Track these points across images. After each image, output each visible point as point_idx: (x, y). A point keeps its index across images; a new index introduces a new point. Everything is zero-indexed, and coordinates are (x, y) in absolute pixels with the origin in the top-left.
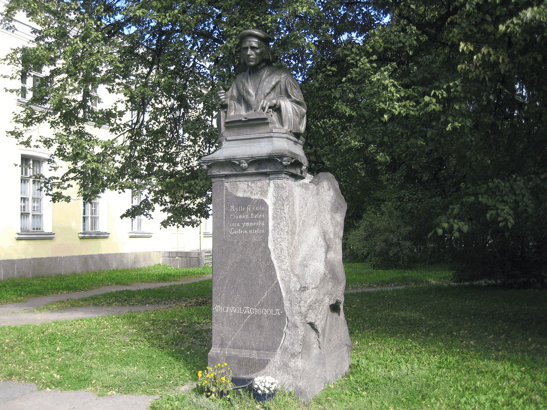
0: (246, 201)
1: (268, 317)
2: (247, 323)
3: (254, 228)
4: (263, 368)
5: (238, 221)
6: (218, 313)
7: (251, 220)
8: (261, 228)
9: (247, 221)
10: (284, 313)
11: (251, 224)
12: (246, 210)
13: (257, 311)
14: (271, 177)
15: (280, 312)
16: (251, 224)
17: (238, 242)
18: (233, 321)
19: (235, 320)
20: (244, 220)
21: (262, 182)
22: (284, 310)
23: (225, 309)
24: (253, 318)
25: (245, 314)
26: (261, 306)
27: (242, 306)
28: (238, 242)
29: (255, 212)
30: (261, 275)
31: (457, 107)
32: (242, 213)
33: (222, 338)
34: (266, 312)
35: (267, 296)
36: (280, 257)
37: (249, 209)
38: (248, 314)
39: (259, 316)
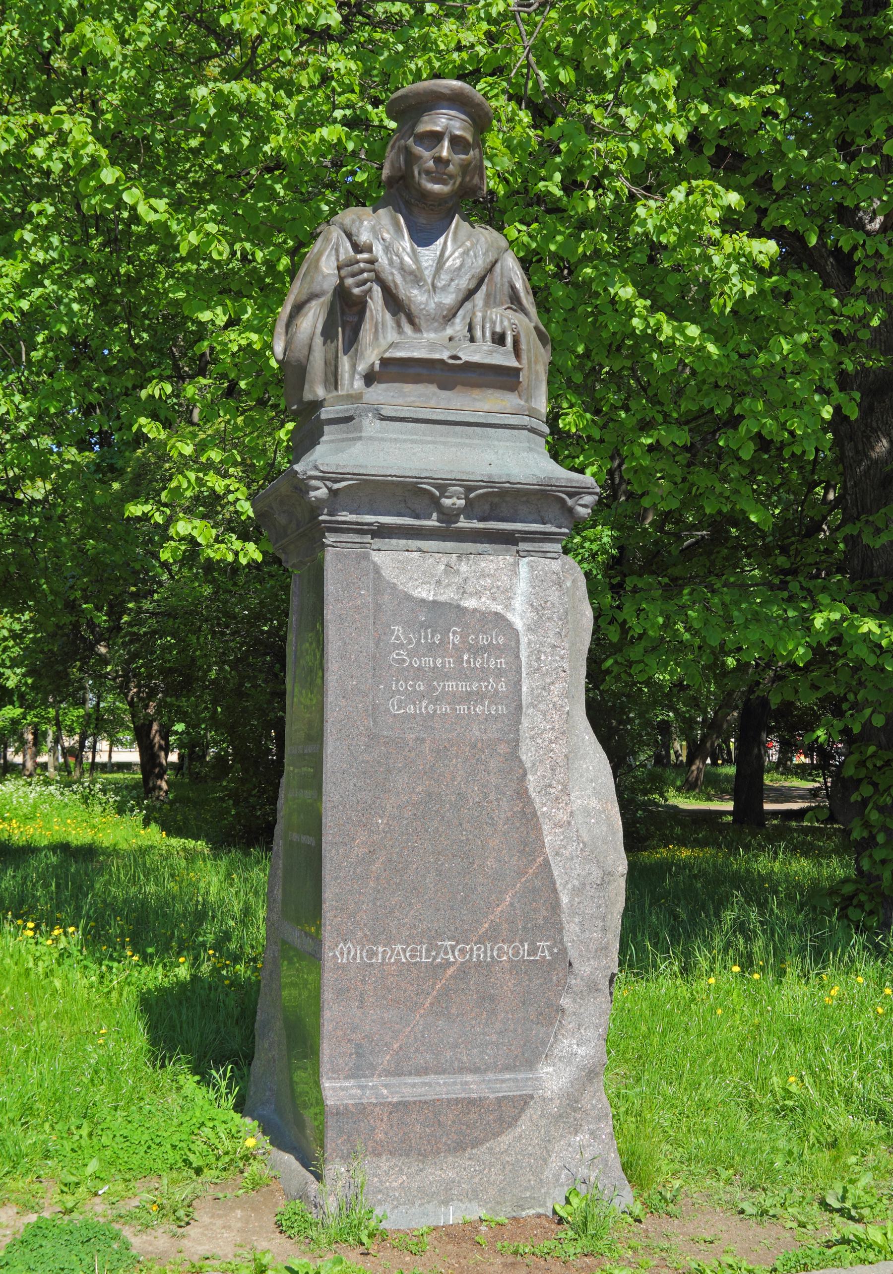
0: (441, 613)
1: (515, 967)
2: (445, 993)
3: (480, 696)
4: (510, 1125)
5: (419, 673)
6: (343, 968)
7: (463, 675)
8: (495, 697)
9: (447, 677)
10: (564, 951)
11: (463, 687)
12: (444, 642)
13: (478, 952)
14: (522, 546)
15: (550, 948)
16: (463, 687)
17: (420, 740)
18: (399, 988)
19: (403, 985)
20: (442, 674)
21: (495, 561)
22: (561, 941)
23: (372, 954)
24: (464, 971)
25: (440, 965)
26: (492, 936)
27: (432, 939)
28: (420, 740)
29: (477, 651)
30: (494, 843)
31: (145, 335)
32: (431, 649)
33: (359, 1046)
34: (505, 952)
35: (512, 904)
36: (550, 786)
37: (454, 639)
38: (449, 964)
39: (486, 967)
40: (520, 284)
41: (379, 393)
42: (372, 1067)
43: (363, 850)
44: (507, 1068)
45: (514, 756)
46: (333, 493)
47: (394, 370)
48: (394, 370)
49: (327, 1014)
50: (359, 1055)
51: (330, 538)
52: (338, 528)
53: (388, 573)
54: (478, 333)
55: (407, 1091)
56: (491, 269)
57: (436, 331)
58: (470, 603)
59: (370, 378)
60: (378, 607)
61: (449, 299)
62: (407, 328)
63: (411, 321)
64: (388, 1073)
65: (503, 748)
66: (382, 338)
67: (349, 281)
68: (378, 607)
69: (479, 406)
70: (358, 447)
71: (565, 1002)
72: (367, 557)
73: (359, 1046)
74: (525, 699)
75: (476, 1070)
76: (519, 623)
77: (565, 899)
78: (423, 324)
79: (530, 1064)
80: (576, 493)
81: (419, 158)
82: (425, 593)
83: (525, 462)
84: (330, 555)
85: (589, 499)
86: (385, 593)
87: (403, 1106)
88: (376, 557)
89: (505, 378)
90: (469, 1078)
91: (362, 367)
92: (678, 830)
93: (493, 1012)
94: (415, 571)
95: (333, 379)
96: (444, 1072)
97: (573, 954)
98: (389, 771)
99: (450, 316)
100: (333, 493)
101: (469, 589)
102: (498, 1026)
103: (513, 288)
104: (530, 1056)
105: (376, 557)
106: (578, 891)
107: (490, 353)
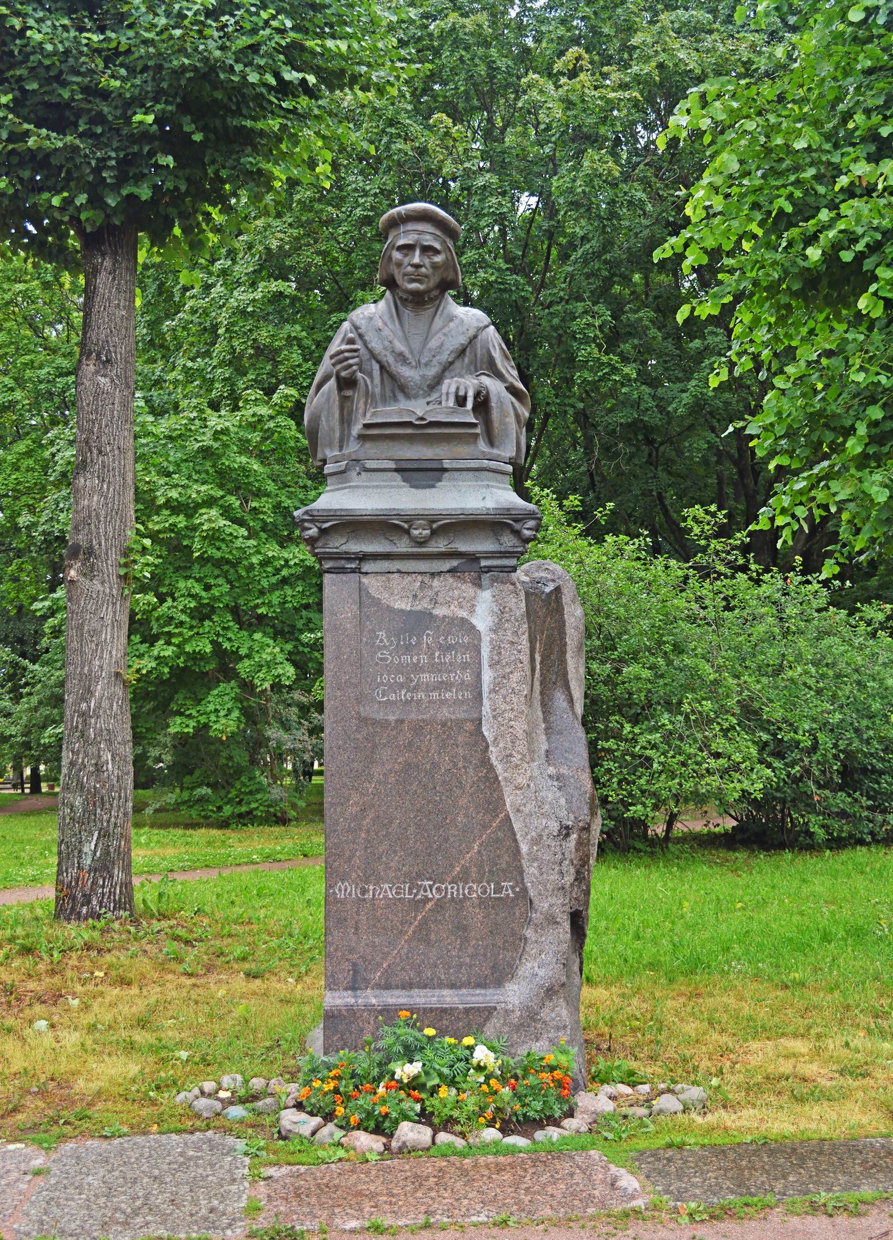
2: (425, 921)
26: (464, 877)
33: (354, 965)
48: (374, 434)
58: (440, 612)
64: (379, 986)
65: (469, 726)
71: (529, 933)
73: (354, 965)
75: (452, 986)
77: (524, 848)
82: (404, 605)
97: (532, 893)
101: (440, 600)
106: (537, 841)
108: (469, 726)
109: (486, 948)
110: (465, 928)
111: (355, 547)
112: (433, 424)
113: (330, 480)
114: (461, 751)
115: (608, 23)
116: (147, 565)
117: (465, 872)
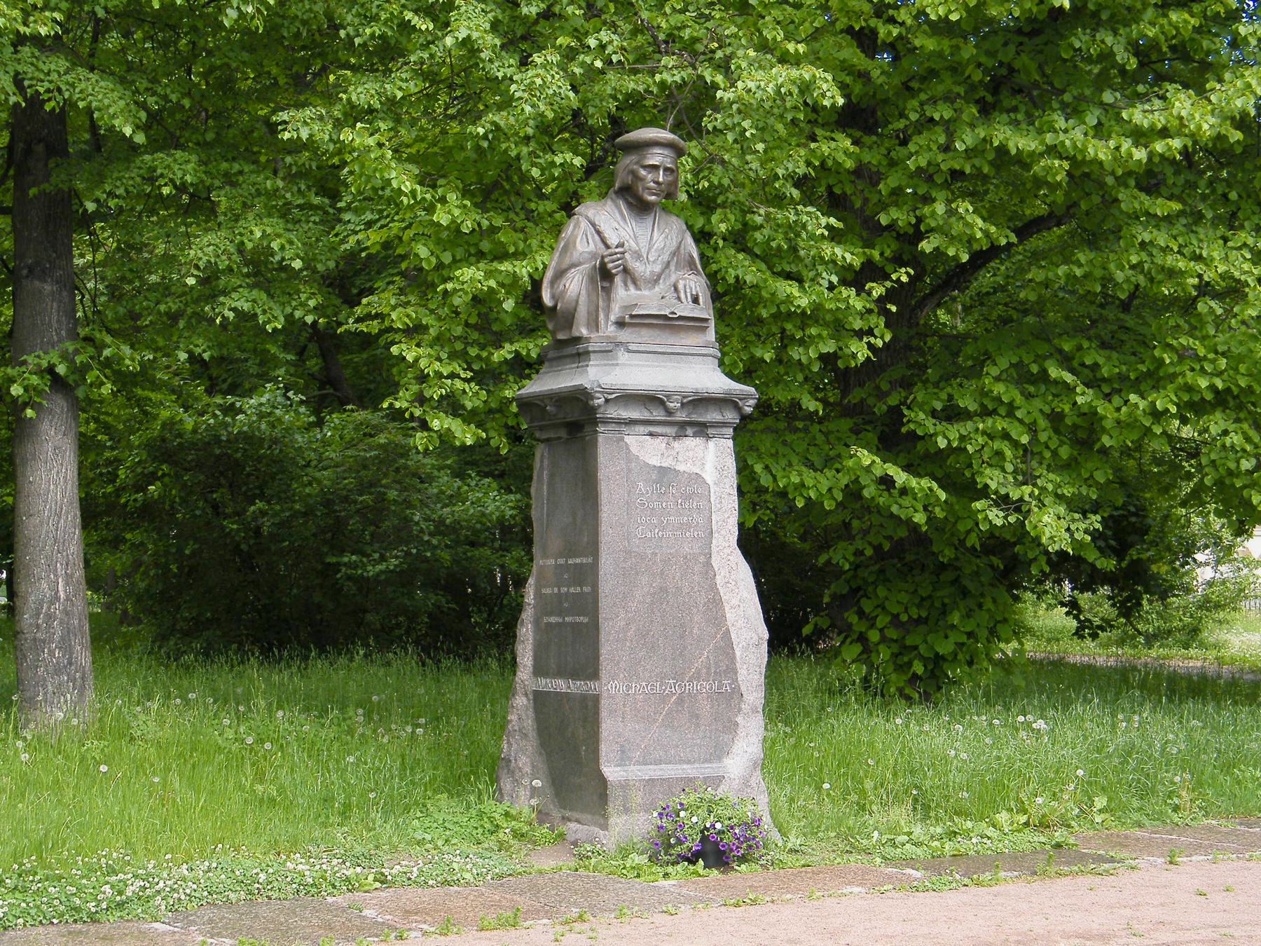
0: (664, 474)
2: (670, 712)
14: (710, 431)
21: (692, 444)
26: (697, 676)
33: (622, 746)
40: (695, 255)
41: (624, 335)
42: (630, 759)
43: (623, 623)
44: (706, 761)
45: (708, 564)
46: (607, 401)
47: (633, 321)
48: (633, 321)
49: (604, 726)
50: (623, 752)
51: (601, 428)
52: (606, 422)
53: (634, 450)
54: (682, 295)
55: (652, 773)
56: (679, 248)
57: (650, 289)
58: (681, 468)
59: (621, 324)
60: (629, 470)
61: (658, 268)
62: (631, 287)
63: (634, 282)
64: (639, 763)
65: (702, 559)
66: (623, 294)
67: (606, 260)
68: (629, 470)
69: (683, 342)
70: (617, 370)
71: (739, 719)
72: (622, 439)
73: (622, 746)
74: (714, 528)
75: (689, 762)
76: (709, 480)
77: (738, 654)
78: (643, 287)
79: (720, 759)
80: (745, 397)
81: (642, 179)
82: (655, 461)
83: (714, 381)
84: (601, 438)
85: (752, 402)
86: (633, 459)
87: (651, 781)
88: (627, 439)
89: (697, 324)
90: (685, 766)
91: (613, 318)
92: (1035, 93)
93: (698, 725)
94: (648, 449)
95: (594, 324)
96: (670, 763)
97: (743, 689)
98: (637, 573)
99: (656, 281)
100: (607, 401)
101: (680, 459)
102: (701, 734)
103: (692, 257)
104: (720, 752)
105: (627, 439)
106: (746, 649)
107: (692, 310)
108: (702, 559)
109: (711, 731)
110: (697, 716)
111: (626, 414)
112: (681, 318)
113: (592, 356)
114: (696, 577)
115: (1132, 251)
116: (901, 506)
117: (698, 672)
